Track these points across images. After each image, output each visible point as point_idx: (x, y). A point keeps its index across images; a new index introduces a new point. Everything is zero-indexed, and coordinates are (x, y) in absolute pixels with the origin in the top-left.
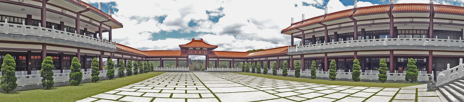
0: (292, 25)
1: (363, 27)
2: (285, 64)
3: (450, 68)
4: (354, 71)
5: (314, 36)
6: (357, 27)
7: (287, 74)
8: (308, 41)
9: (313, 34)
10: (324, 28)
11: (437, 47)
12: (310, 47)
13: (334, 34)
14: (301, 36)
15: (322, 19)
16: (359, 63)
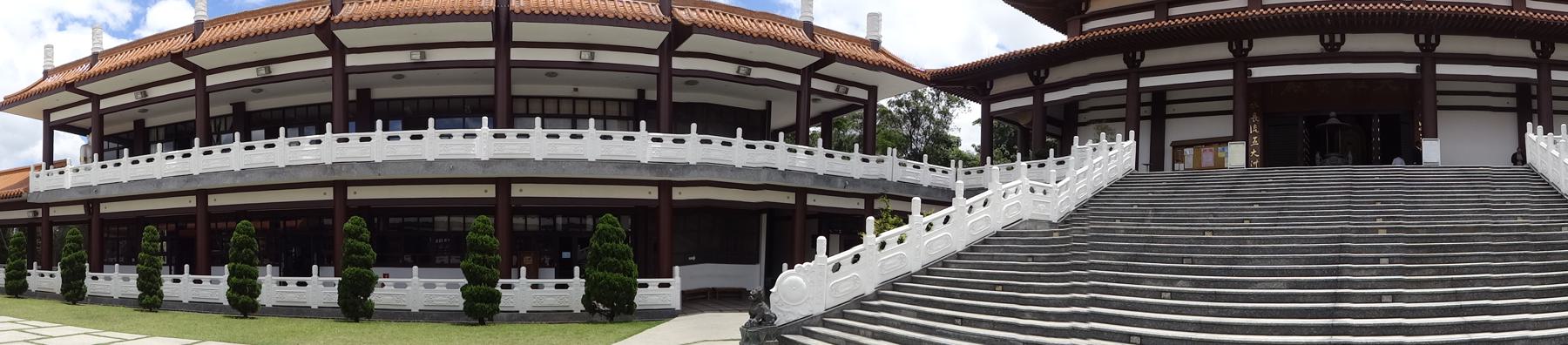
0: (46, 74)
1: (237, 95)
2: (17, 243)
3: (828, 254)
4: (350, 269)
5: (139, 123)
6: (101, 117)
7: (26, 285)
8: (112, 145)
9: (135, 113)
10: (190, 85)
11: (694, 167)
12: (126, 171)
13: (228, 110)
14: (87, 123)
15: (183, 42)
16: (367, 234)
